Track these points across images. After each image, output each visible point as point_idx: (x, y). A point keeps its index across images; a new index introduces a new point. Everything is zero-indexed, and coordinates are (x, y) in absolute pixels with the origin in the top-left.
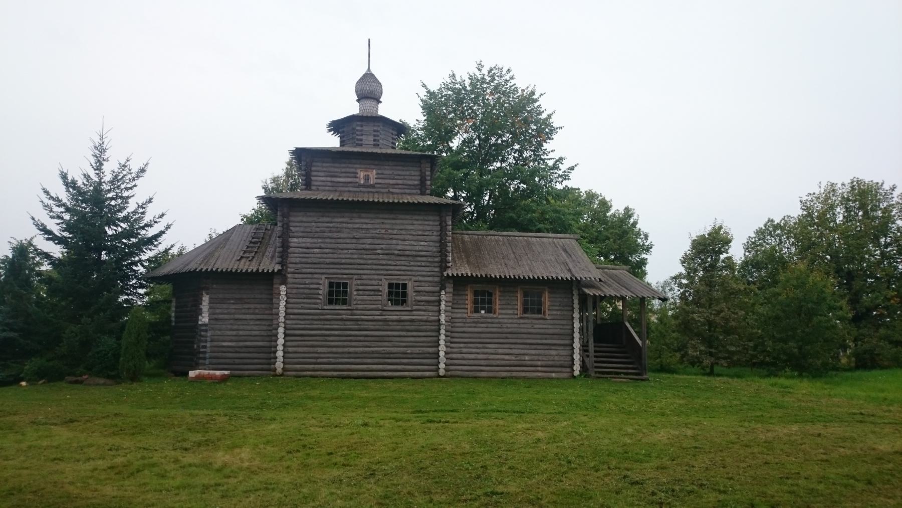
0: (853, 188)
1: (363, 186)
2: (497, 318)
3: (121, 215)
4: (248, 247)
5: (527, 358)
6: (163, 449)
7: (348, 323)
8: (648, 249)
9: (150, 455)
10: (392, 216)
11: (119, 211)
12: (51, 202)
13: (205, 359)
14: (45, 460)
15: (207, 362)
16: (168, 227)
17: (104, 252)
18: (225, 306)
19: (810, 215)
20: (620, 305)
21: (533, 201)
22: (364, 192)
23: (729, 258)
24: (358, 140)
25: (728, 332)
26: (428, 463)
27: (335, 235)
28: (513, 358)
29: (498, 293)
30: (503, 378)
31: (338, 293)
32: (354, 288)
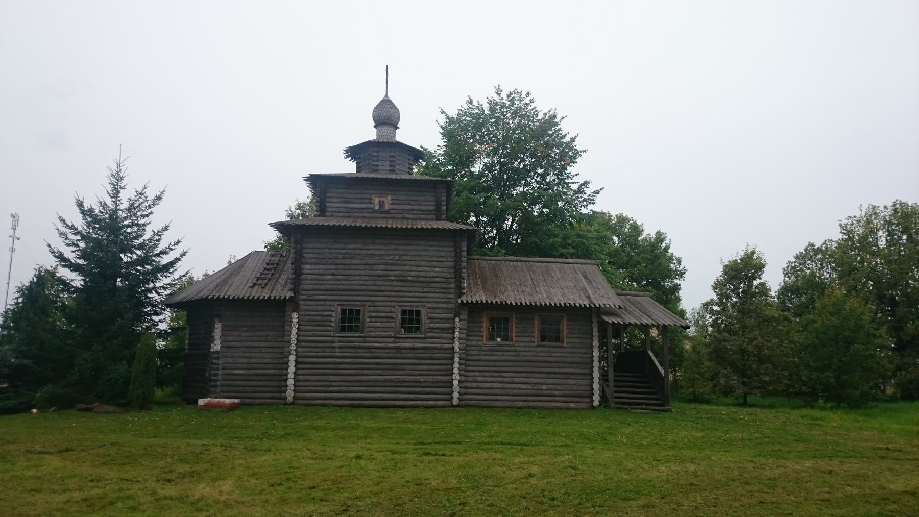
0: (895, 210)
2: (513, 346)
3: (137, 242)
5: (544, 387)
6: (146, 480)
8: (681, 274)
9: (130, 487)
11: (136, 238)
12: (68, 230)
13: (216, 387)
14: (22, 491)
15: (218, 390)
16: (183, 254)
17: (119, 280)
18: (237, 333)
19: (850, 239)
20: (654, 332)
21: (556, 226)
22: (379, 218)
23: (763, 284)
24: (374, 166)
25: (761, 361)
26: (406, 499)
27: (348, 261)
29: (565, 322)
30: (519, 408)
31: (350, 320)
32: (367, 315)
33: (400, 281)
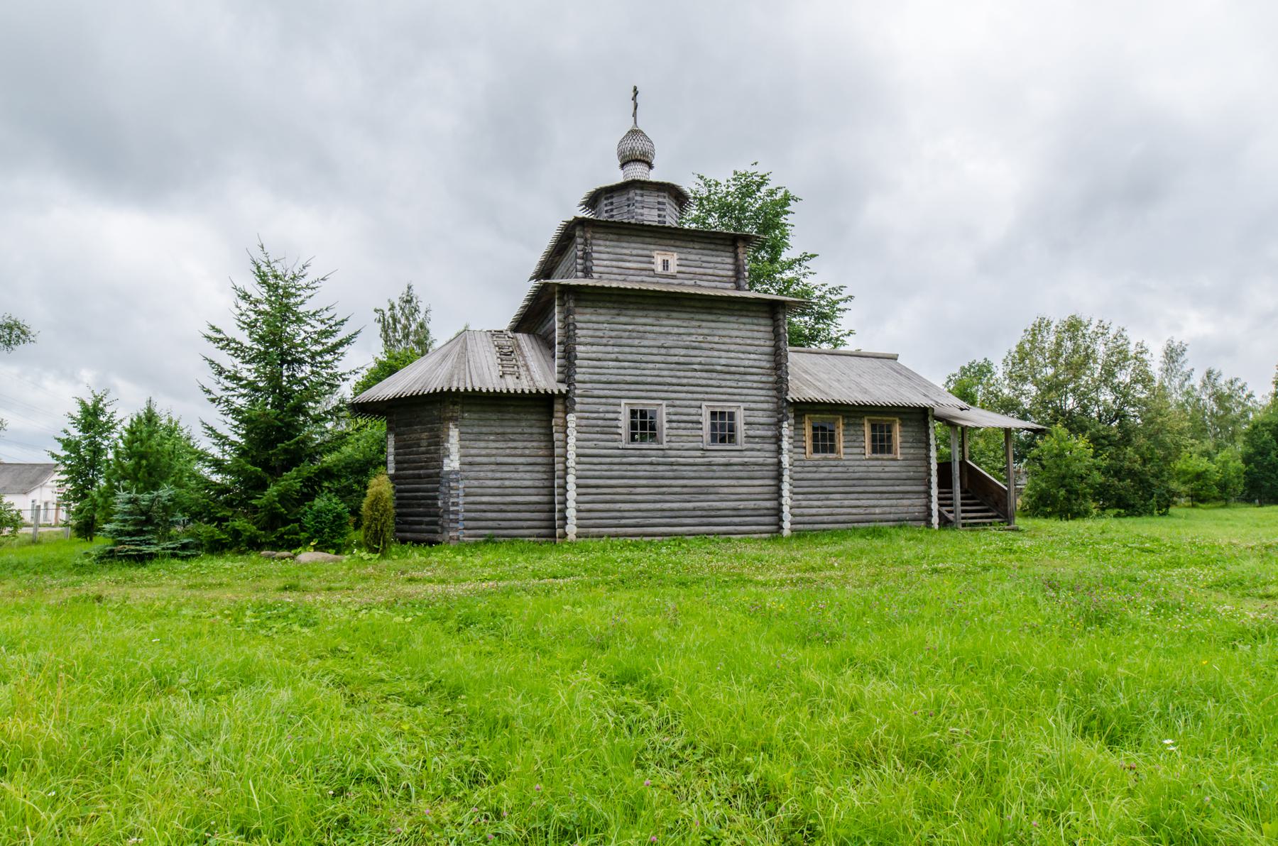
5: (877, 510)
7: (660, 468)
10: (710, 317)
13: (457, 521)
18: (482, 444)
27: (636, 342)
33: (706, 371)
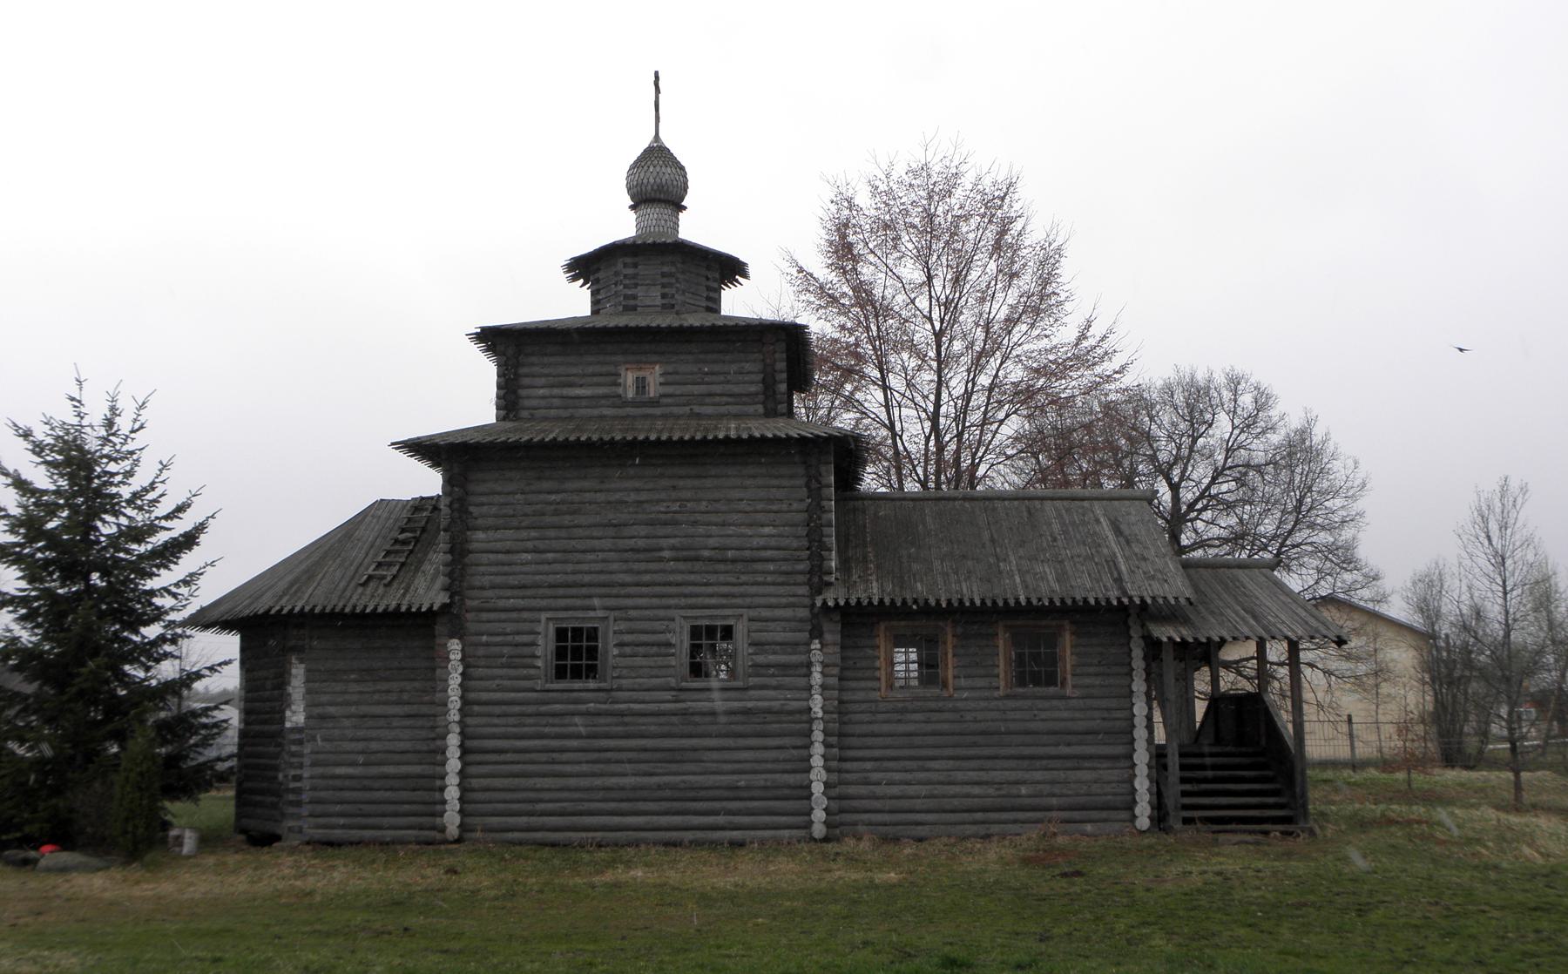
1: (633, 404)
4: (388, 553)
5: (1023, 790)
7: (602, 720)
13: (299, 804)
15: (305, 810)
18: (339, 687)
27: (567, 519)
28: (991, 791)
31: (577, 654)
32: (613, 640)
33: (685, 560)
